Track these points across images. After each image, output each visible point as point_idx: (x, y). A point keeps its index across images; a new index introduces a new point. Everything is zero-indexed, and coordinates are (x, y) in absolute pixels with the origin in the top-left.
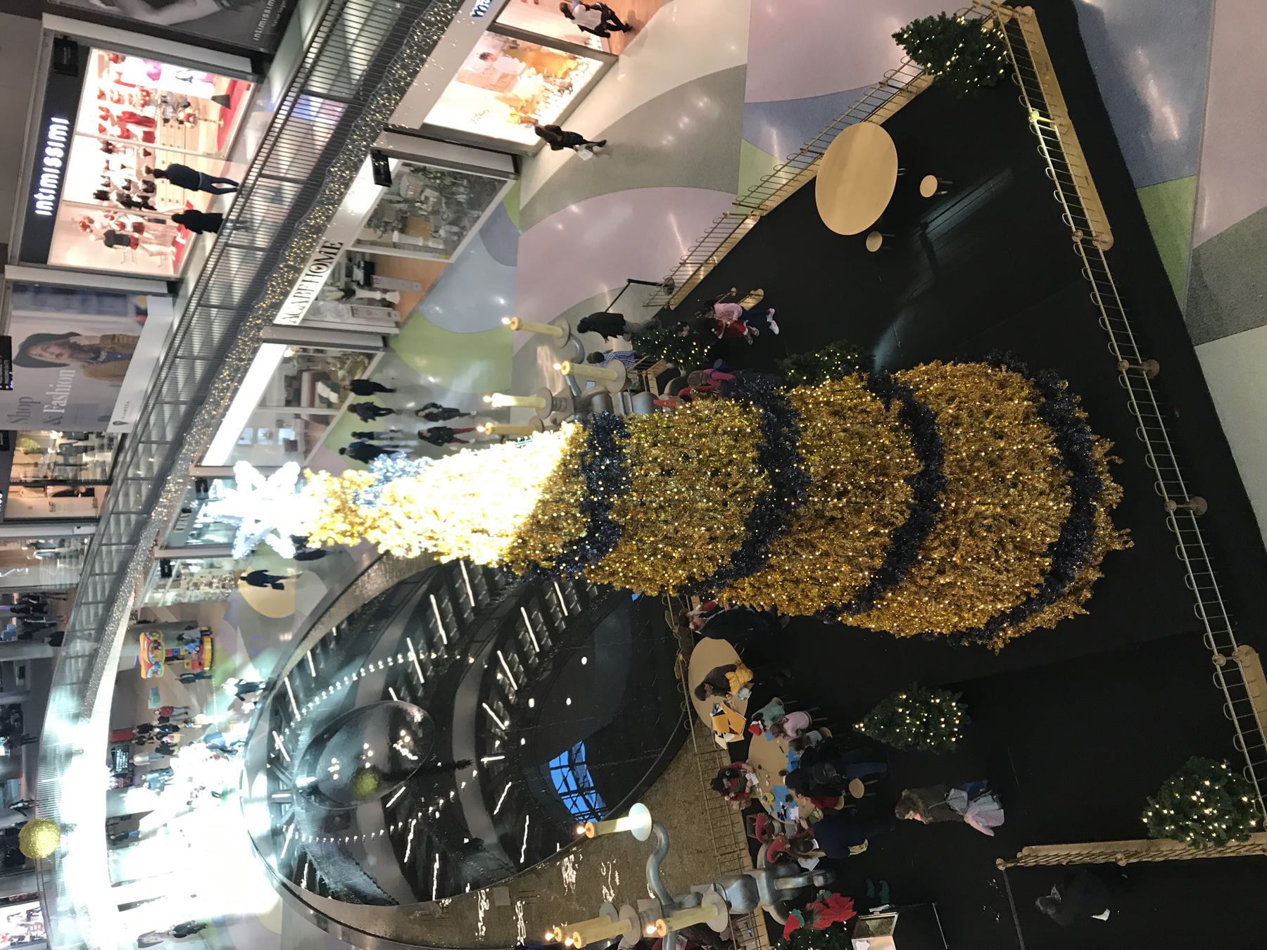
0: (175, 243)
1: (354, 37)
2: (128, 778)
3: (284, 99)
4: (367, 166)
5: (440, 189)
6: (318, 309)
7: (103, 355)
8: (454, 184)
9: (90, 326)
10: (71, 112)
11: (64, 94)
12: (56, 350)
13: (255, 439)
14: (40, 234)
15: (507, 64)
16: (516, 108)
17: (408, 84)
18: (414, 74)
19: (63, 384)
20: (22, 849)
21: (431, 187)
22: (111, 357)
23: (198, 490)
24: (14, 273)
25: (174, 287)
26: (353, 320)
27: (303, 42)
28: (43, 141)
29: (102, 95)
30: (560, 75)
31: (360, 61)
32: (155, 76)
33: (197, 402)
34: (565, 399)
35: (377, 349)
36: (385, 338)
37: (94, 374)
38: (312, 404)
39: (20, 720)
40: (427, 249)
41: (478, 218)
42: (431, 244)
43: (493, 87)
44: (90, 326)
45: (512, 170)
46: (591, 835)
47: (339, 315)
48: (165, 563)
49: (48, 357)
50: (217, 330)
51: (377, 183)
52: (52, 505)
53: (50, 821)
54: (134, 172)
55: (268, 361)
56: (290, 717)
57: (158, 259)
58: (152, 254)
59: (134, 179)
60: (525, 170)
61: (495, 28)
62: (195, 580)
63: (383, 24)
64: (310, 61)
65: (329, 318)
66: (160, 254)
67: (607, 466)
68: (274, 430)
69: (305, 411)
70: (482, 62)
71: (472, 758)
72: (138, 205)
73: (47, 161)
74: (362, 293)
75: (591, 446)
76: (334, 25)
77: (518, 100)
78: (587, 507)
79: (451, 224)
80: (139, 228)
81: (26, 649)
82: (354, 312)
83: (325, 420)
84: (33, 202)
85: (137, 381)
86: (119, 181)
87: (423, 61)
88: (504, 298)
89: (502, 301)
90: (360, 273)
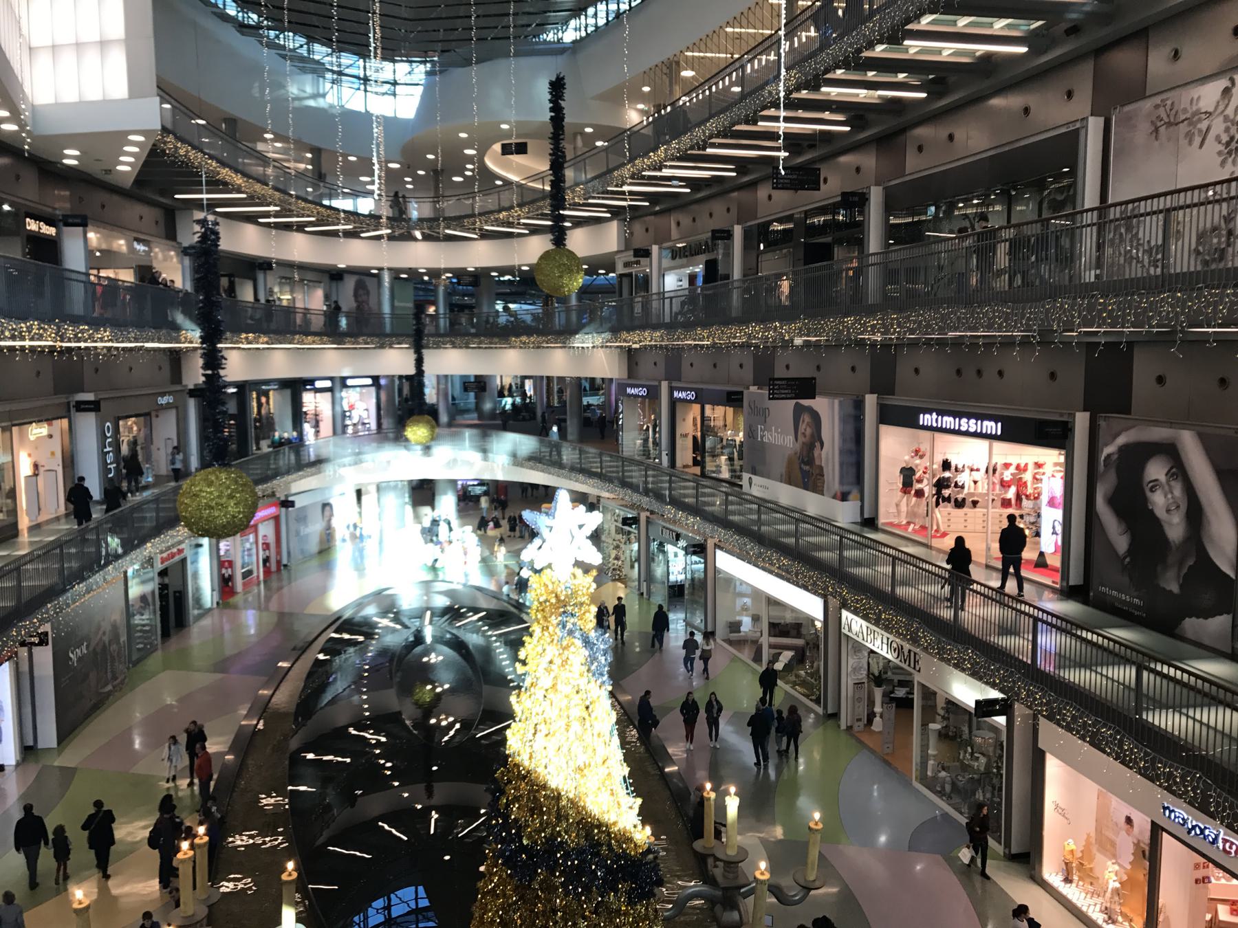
0: (909, 523)
1: (1104, 672)
2: (466, 499)
3: (1048, 613)
4: (995, 694)
5: (988, 772)
6: (860, 651)
7: (807, 468)
8: (994, 788)
9: (830, 455)
10: (1006, 437)
11: (1019, 431)
12: (809, 431)
13: (742, 595)
14: (906, 418)
15: (1126, 845)
16: (1081, 858)
17: (1059, 725)
18: (1069, 729)
19: (781, 437)
20: (415, 417)
21: (988, 765)
22: (805, 473)
23: (694, 546)
24: (871, 401)
25: (870, 523)
26: (851, 683)
27: (1180, 660)
28: (981, 417)
29: (1038, 465)
30: (1125, 910)
31: (1167, 721)
32: (1052, 503)
33: (760, 539)
34: (737, 877)
35: (825, 708)
36: (835, 716)
37: (790, 462)
38: (771, 646)
39: (524, 419)
40: (924, 758)
41: (961, 813)
42: (931, 762)
43: (1099, 830)
44: (830, 455)
45: (1014, 851)
46: (284, 877)
47: (854, 669)
48: (635, 520)
49: (802, 427)
50: (825, 555)
51: (977, 702)
52: (686, 436)
53: (433, 438)
54: (972, 490)
55: (810, 605)
56: (494, 626)
57: (893, 510)
58: (897, 505)
59: (966, 491)
60: (1014, 865)
61: (1156, 830)
62: (622, 546)
63: (1217, 750)
64: (1084, 635)
65: (851, 662)
66: (899, 512)
67: (594, 872)
68: (751, 612)
69: (765, 640)
70: (1123, 819)
71: (435, 800)
72: (939, 493)
73: (973, 421)
74: (878, 693)
75: (619, 857)
76: (1116, 655)
77: (1091, 860)
78: (552, 845)
79: (953, 784)
80: (920, 493)
81: (575, 421)
82: (858, 685)
83: (757, 658)
84: (930, 412)
85: (786, 494)
86: (964, 478)
87: (1083, 738)
88: (889, 842)
89: (883, 839)
90: (896, 690)
